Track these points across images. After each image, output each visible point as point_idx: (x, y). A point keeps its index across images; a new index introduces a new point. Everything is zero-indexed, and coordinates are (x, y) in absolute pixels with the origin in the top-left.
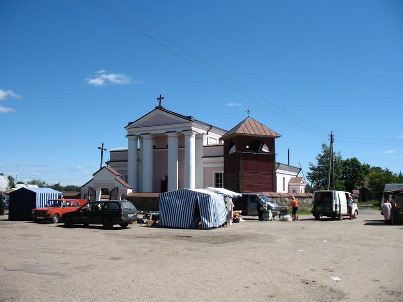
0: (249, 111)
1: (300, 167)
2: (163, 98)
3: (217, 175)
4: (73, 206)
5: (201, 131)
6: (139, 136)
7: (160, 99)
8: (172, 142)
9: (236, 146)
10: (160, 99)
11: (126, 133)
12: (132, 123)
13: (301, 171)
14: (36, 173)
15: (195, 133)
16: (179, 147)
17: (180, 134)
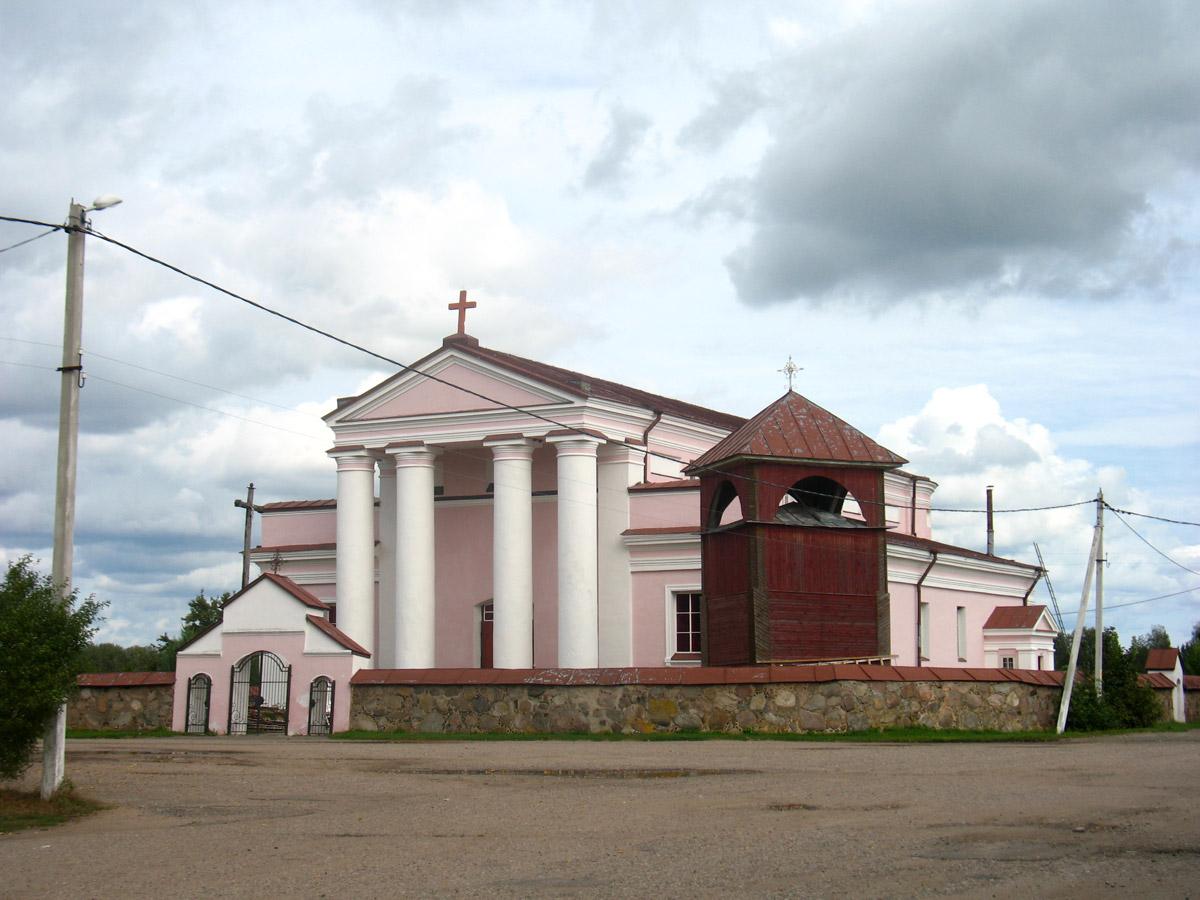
0: (790, 370)
1: (1038, 565)
2: (473, 305)
3: (682, 599)
4: (345, 736)
5: (617, 431)
6: (382, 450)
7: (462, 306)
8: (513, 478)
9: (740, 498)
10: (462, 306)
11: (329, 439)
12: (352, 401)
13: (1042, 581)
14: (1099, 673)
15: (596, 441)
16: (331, 505)
17: (540, 445)
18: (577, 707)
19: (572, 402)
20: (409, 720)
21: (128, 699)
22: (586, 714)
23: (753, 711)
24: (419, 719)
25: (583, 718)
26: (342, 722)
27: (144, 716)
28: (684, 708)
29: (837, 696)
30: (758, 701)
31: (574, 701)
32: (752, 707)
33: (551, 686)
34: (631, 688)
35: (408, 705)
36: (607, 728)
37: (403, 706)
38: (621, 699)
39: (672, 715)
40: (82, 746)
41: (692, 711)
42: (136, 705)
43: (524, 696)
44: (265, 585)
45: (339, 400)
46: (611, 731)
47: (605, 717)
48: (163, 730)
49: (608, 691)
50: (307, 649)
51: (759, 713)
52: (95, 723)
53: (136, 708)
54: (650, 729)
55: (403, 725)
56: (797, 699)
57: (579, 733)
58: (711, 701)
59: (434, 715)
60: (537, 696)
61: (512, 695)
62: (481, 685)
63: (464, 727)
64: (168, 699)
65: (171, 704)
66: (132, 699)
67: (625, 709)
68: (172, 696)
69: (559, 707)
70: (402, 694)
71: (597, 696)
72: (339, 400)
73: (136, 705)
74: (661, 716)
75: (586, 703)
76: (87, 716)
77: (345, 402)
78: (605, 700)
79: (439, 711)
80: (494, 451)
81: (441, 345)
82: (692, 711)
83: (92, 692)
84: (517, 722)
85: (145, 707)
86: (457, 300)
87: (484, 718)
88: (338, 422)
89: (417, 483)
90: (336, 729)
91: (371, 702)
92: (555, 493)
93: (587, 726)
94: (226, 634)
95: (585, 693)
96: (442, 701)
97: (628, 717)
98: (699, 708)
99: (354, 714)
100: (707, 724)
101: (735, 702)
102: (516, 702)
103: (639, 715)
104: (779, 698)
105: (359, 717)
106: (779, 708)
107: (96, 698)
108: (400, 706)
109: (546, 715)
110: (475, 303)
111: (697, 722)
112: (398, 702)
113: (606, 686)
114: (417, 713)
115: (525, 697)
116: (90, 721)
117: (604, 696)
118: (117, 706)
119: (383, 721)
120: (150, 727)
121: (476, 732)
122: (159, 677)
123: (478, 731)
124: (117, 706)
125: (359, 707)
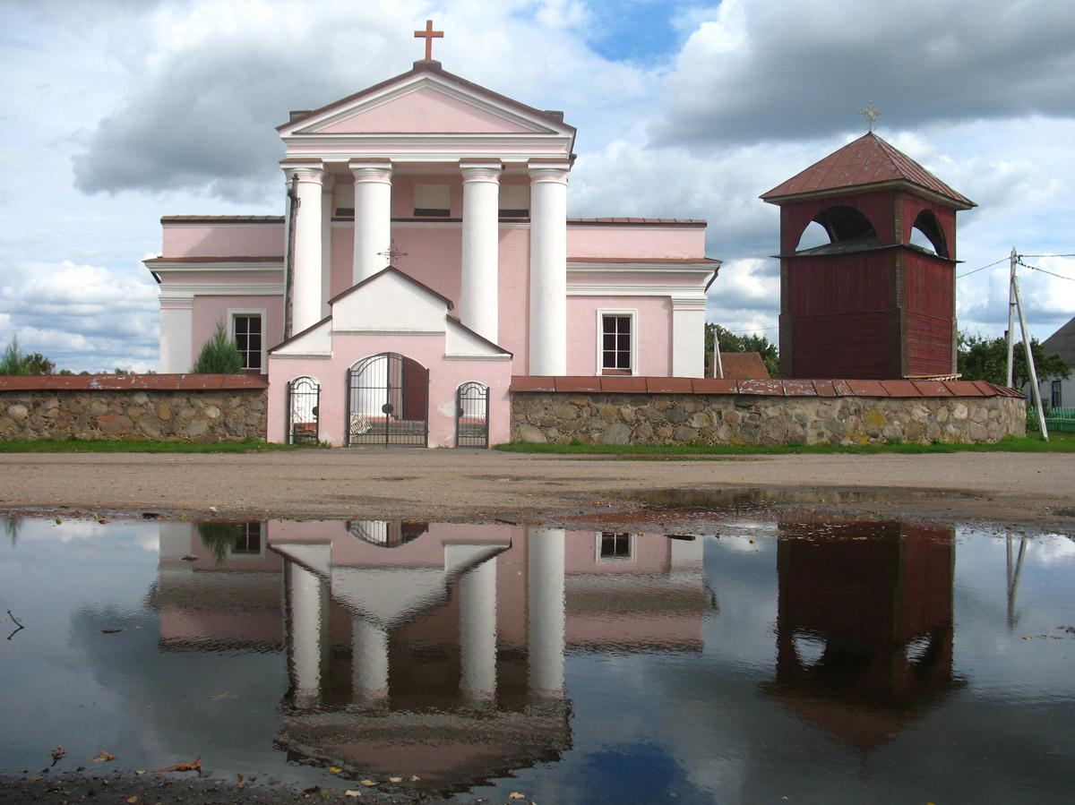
8: (484, 199)
12: (308, 115)
18: (794, 419)
19: (556, 133)
20: (587, 431)
21: (202, 405)
22: (804, 426)
23: (938, 423)
24: (600, 430)
25: (799, 430)
26: (500, 431)
27: (226, 425)
28: (890, 420)
29: (995, 409)
30: (942, 414)
31: (789, 412)
32: (939, 419)
33: (765, 397)
34: (850, 400)
35: (585, 415)
36: (825, 439)
37: (579, 416)
38: (840, 411)
39: (881, 427)
40: (571, 470)
41: (896, 423)
42: (213, 413)
43: (729, 409)
44: (389, 281)
45: (291, 113)
46: (829, 442)
47: (823, 429)
48: (253, 442)
49: (828, 402)
50: (449, 352)
51: (943, 424)
52: (156, 434)
53: (214, 416)
54: (864, 441)
55: (580, 438)
56: (969, 412)
57: (795, 445)
58: (909, 413)
59: (618, 427)
60: (748, 408)
61: (714, 406)
62: (677, 394)
63: (656, 438)
64: (261, 406)
65: (264, 412)
66: (207, 406)
67: (844, 421)
68: (265, 402)
69: (773, 418)
70: (577, 402)
71: (816, 409)
72: (291, 113)
73: (213, 413)
74: (872, 428)
75: (804, 414)
76: (143, 424)
77: (304, 115)
78: (826, 412)
79: (624, 421)
80: (355, 174)
81: (411, 68)
82: (896, 423)
83: (148, 397)
84: (722, 434)
85: (226, 414)
86: (435, 28)
87: (681, 430)
88: (294, 133)
89: (376, 200)
90: (493, 440)
91: (538, 411)
92: (461, 220)
93: (804, 438)
94: (333, 333)
95: (803, 405)
96: (628, 411)
97: (848, 429)
98: (900, 420)
99: (515, 424)
100: (906, 436)
101: (926, 415)
102: (719, 413)
103: (856, 428)
104: (956, 411)
105: (523, 428)
106: (956, 419)
107: (155, 403)
108: (575, 416)
109: (757, 427)
110: (442, 33)
111: (899, 434)
112: (571, 412)
113: (826, 398)
114: (597, 423)
115: (731, 408)
116: (149, 430)
117: (823, 408)
118: (185, 413)
119: (553, 432)
120: (235, 438)
121: (671, 444)
122: (241, 380)
123: (674, 443)
124: (185, 413)
125: (521, 417)
